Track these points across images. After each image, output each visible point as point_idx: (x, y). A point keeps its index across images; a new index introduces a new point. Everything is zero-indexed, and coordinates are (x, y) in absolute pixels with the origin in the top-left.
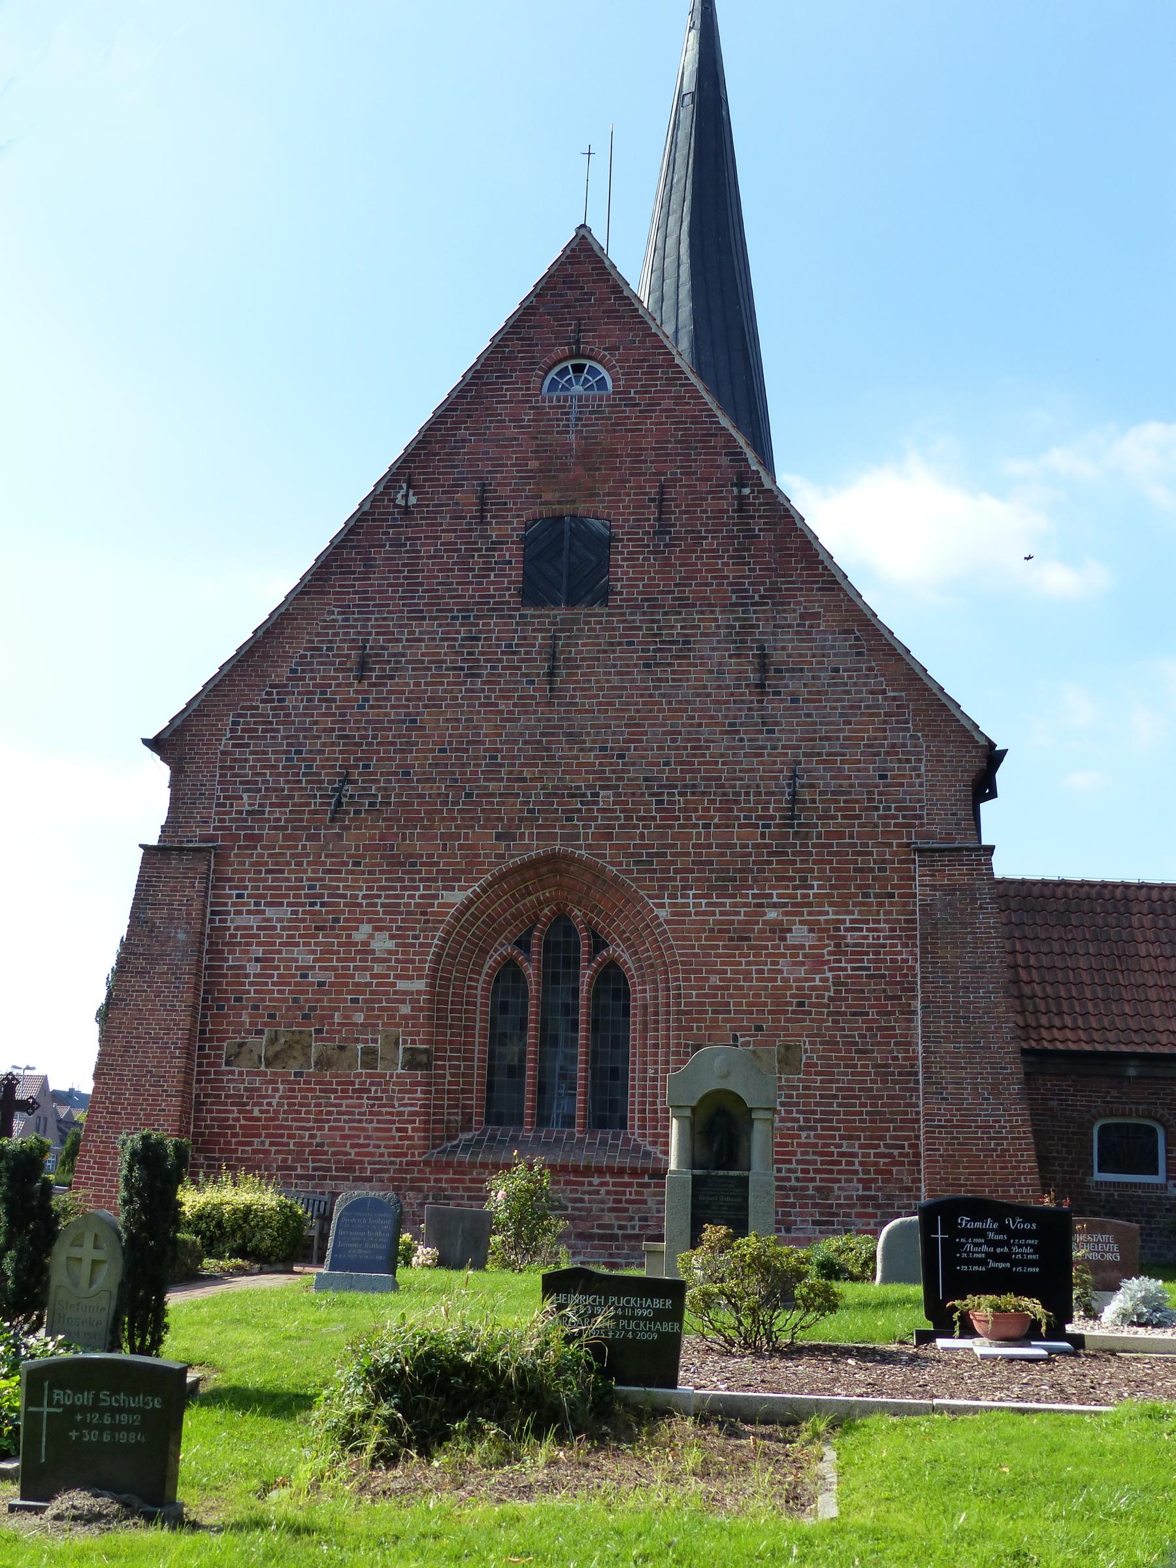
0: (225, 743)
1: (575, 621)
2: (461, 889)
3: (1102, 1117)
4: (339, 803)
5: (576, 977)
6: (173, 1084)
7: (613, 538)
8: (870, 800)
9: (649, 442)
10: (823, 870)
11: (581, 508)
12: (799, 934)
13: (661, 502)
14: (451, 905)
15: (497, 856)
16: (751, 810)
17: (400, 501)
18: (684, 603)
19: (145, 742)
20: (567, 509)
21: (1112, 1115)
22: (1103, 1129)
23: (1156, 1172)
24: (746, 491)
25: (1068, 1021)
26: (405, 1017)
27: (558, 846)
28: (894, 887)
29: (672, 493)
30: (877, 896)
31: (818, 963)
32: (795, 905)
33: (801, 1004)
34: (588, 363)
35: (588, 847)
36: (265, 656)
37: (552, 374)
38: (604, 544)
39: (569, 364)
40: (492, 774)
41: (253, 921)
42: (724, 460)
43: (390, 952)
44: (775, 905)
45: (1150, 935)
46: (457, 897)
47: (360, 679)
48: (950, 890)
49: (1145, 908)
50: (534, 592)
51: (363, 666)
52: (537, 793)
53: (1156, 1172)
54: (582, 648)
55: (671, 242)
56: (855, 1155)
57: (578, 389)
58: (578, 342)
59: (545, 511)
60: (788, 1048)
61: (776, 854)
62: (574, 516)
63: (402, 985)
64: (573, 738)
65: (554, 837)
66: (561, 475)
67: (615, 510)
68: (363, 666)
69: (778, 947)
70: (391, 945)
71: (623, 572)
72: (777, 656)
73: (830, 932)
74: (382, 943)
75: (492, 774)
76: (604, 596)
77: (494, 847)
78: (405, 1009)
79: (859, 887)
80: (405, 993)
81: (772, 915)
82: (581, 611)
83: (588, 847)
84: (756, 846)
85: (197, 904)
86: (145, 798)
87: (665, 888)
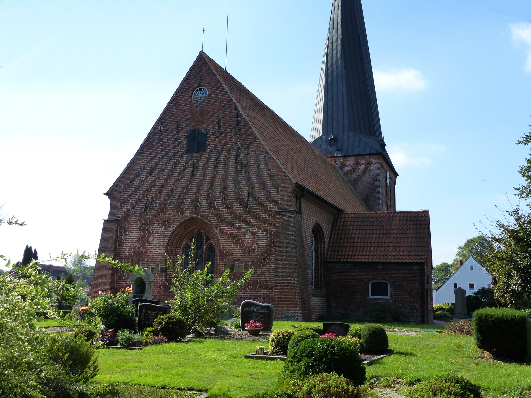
0: (122, 193)
1: (198, 157)
2: (173, 227)
3: (371, 280)
4: (146, 207)
5: (203, 247)
6: (109, 277)
7: (207, 134)
8: (267, 199)
9: (216, 108)
10: (254, 218)
11: (200, 127)
12: (249, 235)
13: (219, 123)
14: (170, 231)
15: (181, 218)
16: (238, 203)
17: (159, 129)
18: (224, 150)
19: (104, 194)
20: (197, 127)
21: (374, 279)
22: (373, 284)
23: (387, 296)
24: (239, 119)
25: (365, 253)
26: (160, 259)
27: (194, 215)
28: (272, 222)
29: (221, 121)
30: (268, 224)
31: (253, 242)
32: (248, 227)
33: (249, 253)
34: (203, 88)
35: (201, 215)
36: (130, 171)
37: (195, 92)
38: (206, 135)
39: (198, 88)
40: (179, 198)
41: (128, 237)
42: (234, 111)
43: (157, 243)
44: (243, 228)
45: (397, 227)
46: (171, 229)
47: (150, 175)
48: (283, 222)
49: (398, 219)
50: (189, 150)
51: (151, 172)
52: (189, 201)
53: (387, 296)
54: (200, 163)
55: (336, 9)
56: (261, 292)
57: (200, 95)
58: (200, 82)
59: (192, 128)
60: (246, 264)
61: (243, 215)
62: (198, 129)
63: (160, 251)
64: (198, 187)
65: (193, 213)
66: (196, 119)
67: (208, 127)
68: (151, 172)
69: (244, 239)
70: (157, 242)
71: (210, 143)
72: (245, 162)
73: (256, 234)
74: (155, 241)
75: (179, 198)
76: (205, 150)
77: (179, 216)
78: (160, 257)
79: (263, 222)
80: (160, 253)
81: (243, 230)
82: (200, 154)
83: (201, 215)
84: (239, 213)
85: (115, 234)
86: (103, 208)
87: (217, 225)
